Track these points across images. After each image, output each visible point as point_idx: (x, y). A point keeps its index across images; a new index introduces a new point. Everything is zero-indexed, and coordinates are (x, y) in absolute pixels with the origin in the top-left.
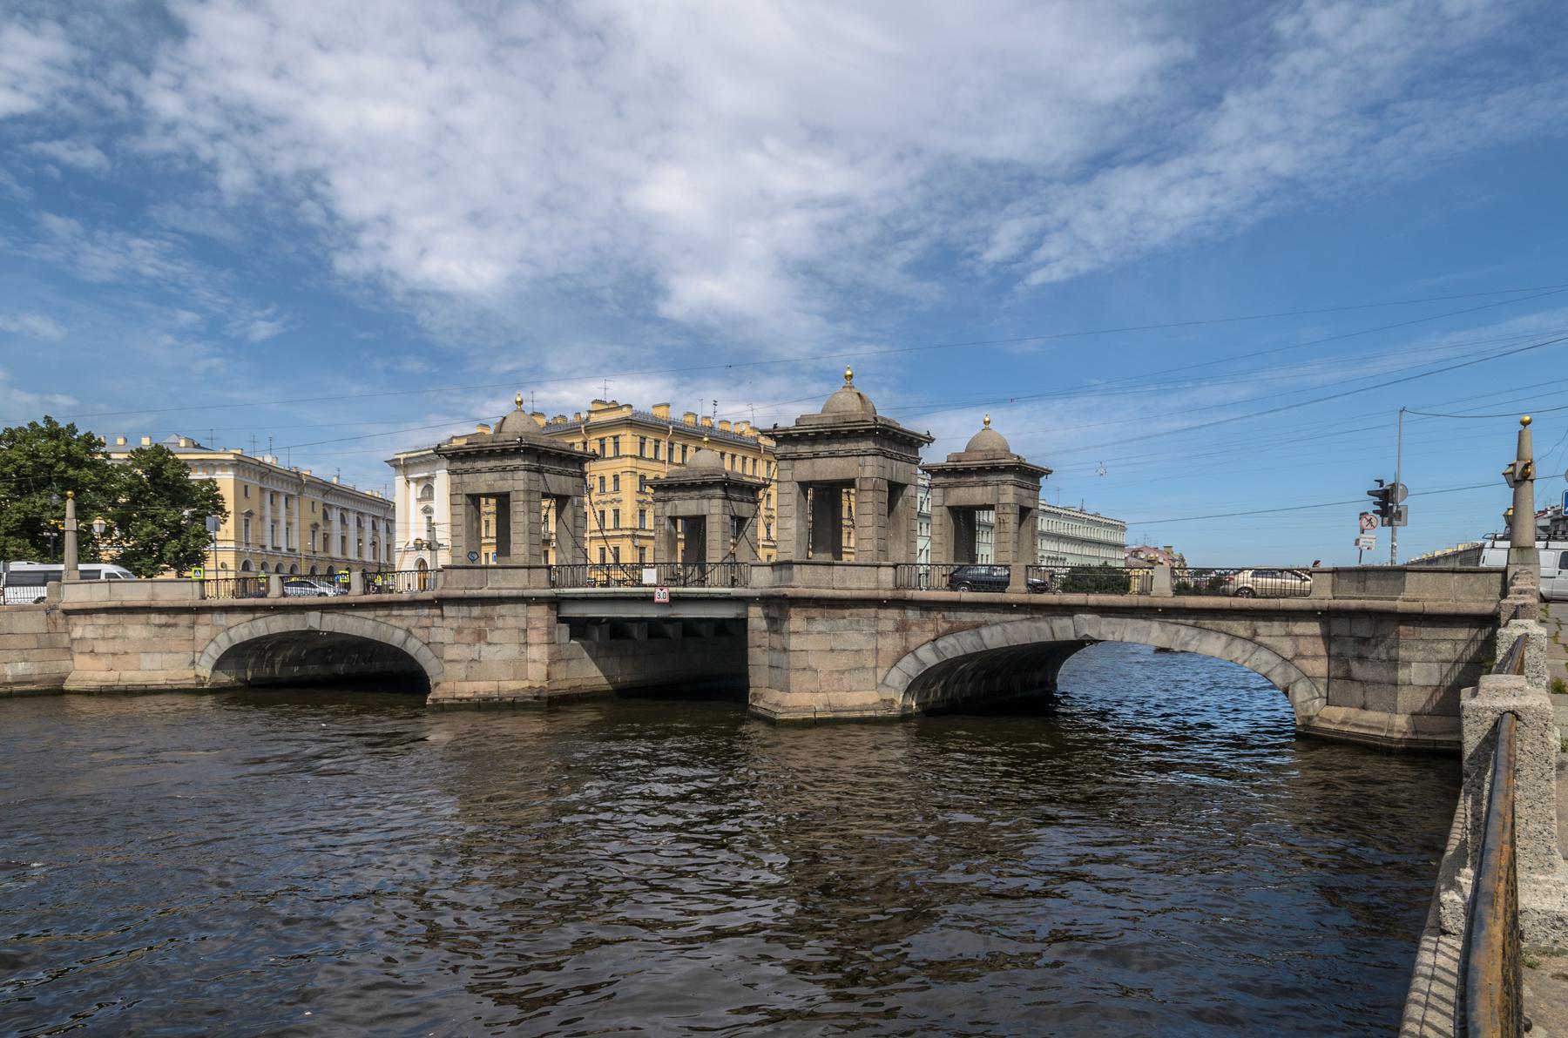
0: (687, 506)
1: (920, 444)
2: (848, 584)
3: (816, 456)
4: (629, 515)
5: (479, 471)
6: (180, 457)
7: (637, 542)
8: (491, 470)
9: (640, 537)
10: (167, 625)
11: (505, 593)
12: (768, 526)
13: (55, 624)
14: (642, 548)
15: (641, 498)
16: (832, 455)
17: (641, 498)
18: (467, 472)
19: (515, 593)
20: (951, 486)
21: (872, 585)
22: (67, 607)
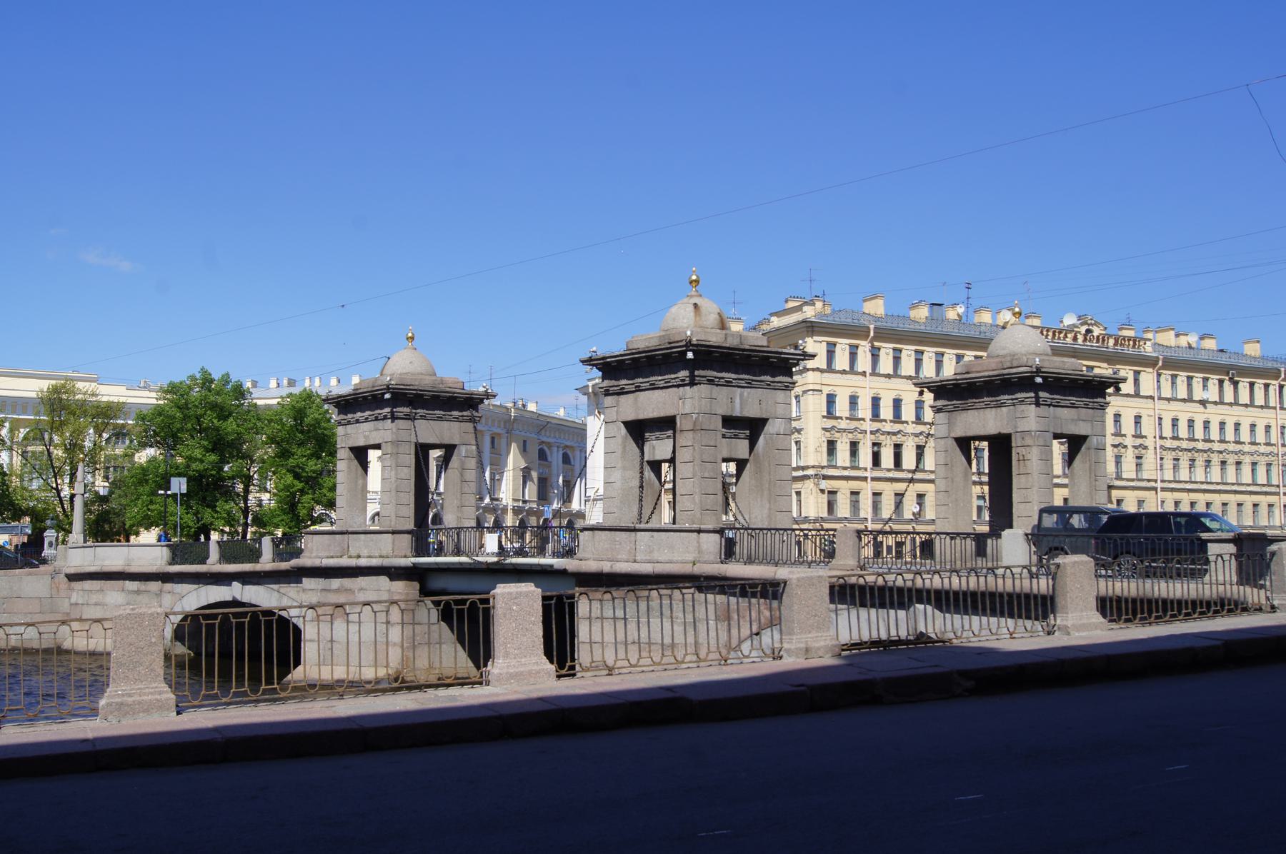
0: (985, 420)
1: (481, 401)
2: (656, 556)
3: (638, 389)
4: (811, 449)
5: (357, 422)
6: (260, 402)
7: (825, 484)
8: (367, 420)
9: (825, 477)
10: (138, 592)
11: (363, 562)
12: (1118, 460)
13: (1267, 598)
14: (832, 493)
15: (829, 424)
16: (653, 387)
17: (829, 424)
18: (349, 423)
19: (375, 562)
20: (956, 409)
21: (690, 557)
22: (72, 571)
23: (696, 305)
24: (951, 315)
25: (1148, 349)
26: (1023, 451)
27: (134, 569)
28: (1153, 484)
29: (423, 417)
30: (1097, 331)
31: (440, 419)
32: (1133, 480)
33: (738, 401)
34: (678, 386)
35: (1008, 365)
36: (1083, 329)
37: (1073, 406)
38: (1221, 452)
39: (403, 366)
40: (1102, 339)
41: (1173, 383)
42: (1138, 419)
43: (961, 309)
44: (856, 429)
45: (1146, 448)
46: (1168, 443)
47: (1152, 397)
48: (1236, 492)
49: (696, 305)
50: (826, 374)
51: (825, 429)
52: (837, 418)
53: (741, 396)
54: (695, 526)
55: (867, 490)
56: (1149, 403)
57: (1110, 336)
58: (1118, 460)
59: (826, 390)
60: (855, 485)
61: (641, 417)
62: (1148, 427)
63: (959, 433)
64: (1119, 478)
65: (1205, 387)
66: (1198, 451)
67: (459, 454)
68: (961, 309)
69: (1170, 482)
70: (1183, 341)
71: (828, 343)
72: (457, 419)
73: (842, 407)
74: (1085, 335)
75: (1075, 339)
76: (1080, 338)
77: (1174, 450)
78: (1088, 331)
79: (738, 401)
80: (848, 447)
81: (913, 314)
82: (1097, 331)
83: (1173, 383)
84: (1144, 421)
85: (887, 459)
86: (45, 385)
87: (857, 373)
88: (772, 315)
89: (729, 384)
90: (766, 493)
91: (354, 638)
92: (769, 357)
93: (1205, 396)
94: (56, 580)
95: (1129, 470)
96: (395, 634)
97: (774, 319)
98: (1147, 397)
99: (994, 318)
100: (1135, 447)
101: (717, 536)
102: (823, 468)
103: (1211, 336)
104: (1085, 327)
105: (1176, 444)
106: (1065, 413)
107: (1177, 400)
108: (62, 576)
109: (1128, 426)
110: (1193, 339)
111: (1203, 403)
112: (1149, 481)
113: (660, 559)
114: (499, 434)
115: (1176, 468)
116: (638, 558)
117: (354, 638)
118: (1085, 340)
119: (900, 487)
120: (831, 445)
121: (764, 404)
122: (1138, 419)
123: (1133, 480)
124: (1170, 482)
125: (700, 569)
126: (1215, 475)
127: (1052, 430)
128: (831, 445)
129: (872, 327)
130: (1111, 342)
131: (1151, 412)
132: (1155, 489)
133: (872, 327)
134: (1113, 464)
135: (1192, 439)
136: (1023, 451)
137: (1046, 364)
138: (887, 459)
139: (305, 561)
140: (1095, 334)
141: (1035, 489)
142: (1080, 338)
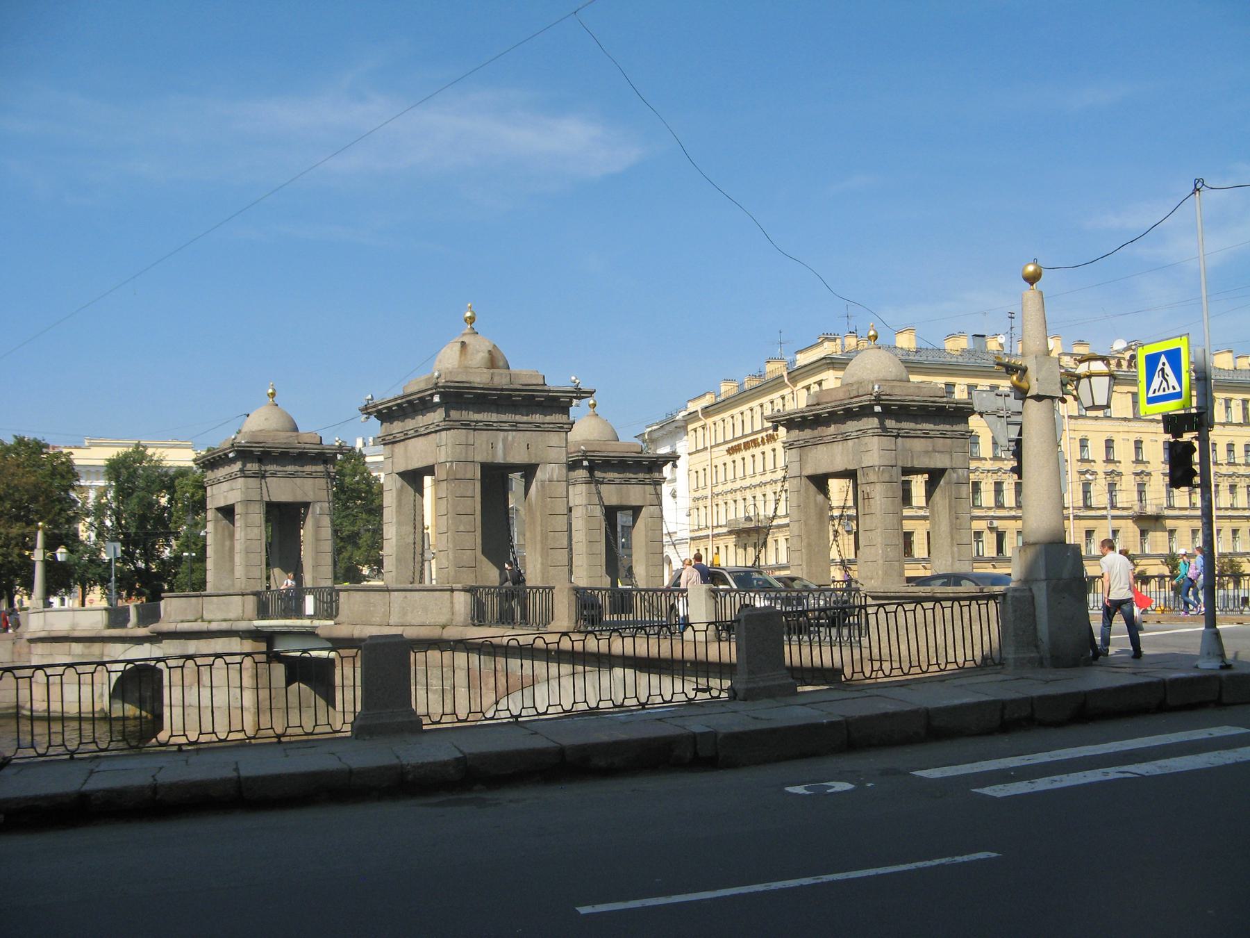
2: (410, 618)
11: (214, 626)
12: (1112, 488)
19: (225, 626)
21: (443, 619)
23: (463, 344)
26: (867, 489)
27: (77, 634)
29: (274, 475)
31: (293, 475)
32: (1186, 509)
33: (500, 445)
34: (436, 432)
35: (854, 393)
36: (1127, 355)
37: (926, 436)
39: (259, 423)
41: (1228, 407)
42: (1109, 444)
43: (1002, 339)
49: (463, 344)
53: (505, 440)
54: (447, 586)
56: (1124, 426)
58: (1112, 488)
61: (410, 468)
63: (810, 471)
64: (1170, 507)
67: (314, 513)
68: (1002, 339)
69: (1226, 509)
72: (310, 475)
74: (1130, 362)
75: (1119, 365)
76: (1124, 364)
77: (1230, 476)
79: (500, 445)
81: (949, 345)
83: (1228, 407)
86: (112, 453)
88: (797, 352)
89: (488, 427)
90: (539, 546)
91: (206, 702)
92: (559, 397)
94: (18, 645)
96: (249, 699)
97: (798, 356)
101: (468, 595)
104: (1131, 352)
105: (1232, 470)
106: (918, 445)
107: (1231, 424)
108: (24, 641)
109: (1096, 451)
112: (1124, 509)
113: (414, 622)
116: (391, 622)
117: (206, 702)
118: (1129, 366)
121: (532, 449)
122: (1109, 444)
123: (1186, 509)
124: (1226, 509)
125: (452, 633)
127: (900, 464)
136: (867, 489)
137: (897, 391)
139: (164, 626)
141: (879, 530)
142: (1124, 364)
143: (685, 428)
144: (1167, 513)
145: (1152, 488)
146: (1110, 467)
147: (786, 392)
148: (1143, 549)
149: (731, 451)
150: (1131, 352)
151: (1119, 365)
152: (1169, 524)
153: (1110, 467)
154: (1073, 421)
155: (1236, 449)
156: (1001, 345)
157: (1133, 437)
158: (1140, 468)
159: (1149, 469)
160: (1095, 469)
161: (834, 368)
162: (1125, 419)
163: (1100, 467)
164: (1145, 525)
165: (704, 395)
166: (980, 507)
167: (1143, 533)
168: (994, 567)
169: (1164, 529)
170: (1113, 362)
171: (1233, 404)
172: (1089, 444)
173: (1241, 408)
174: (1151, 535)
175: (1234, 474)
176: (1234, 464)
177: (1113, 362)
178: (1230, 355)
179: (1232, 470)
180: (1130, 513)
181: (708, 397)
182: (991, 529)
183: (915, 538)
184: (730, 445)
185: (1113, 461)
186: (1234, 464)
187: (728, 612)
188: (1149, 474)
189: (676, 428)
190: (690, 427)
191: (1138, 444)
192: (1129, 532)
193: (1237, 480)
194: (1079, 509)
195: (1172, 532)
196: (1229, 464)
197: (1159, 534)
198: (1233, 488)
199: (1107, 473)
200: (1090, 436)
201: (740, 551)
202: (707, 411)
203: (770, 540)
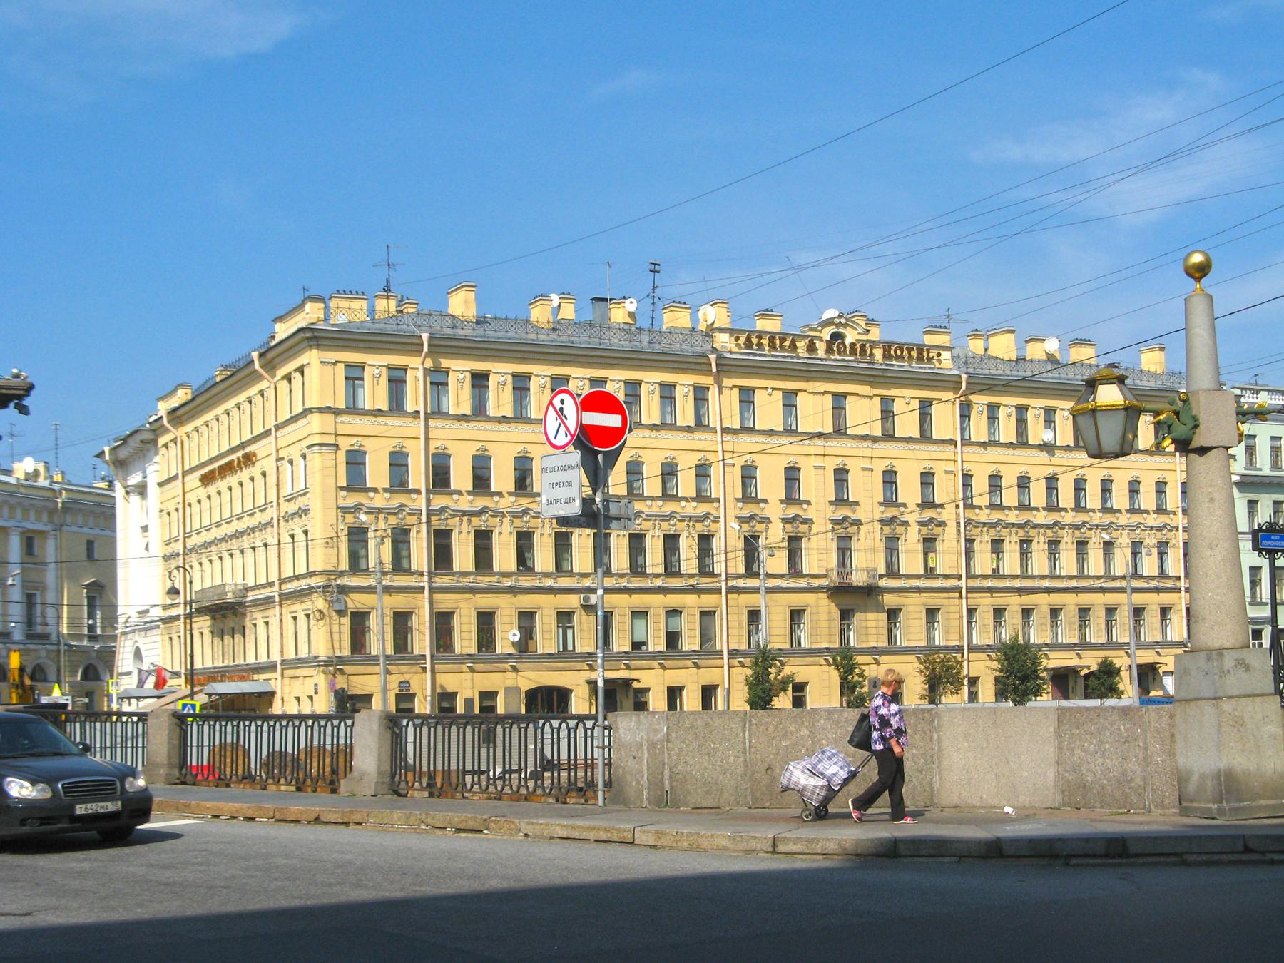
15: (351, 500)
24: (618, 315)
25: (946, 363)
28: (954, 582)
30: (851, 337)
38: (1077, 527)
40: (861, 349)
42: (927, 479)
43: (631, 305)
44: (401, 508)
45: (942, 524)
46: (983, 516)
47: (952, 442)
48: (1048, 591)
50: (513, 426)
51: (834, 522)
52: (368, 490)
55: (547, 608)
56: (866, 448)
57: (874, 344)
58: (929, 543)
59: (345, 444)
60: (400, 602)
62: (947, 489)
65: (1049, 422)
66: (1036, 526)
68: (631, 305)
70: (1035, 351)
71: (348, 365)
73: (377, 473)
75: (811, 348)
76: (821, 347)
78: (837, 337)
80: (513, 540)
82: (851, 337)
83: (993, 418)
84: (716, 472)
85: (463, 555)
87: (530, 421)
93: (1048, 436)
95: (910, 561)
97: (278, 327)
98: (943, 442)
99: (694, 317)
100: (742, 520)
102: (342, 574)
103: (1087, 342)
105: (996, 516)
107: (997, 444)
110: (1052, 345)
111: (1049, 448)
112: (946, 577)
114: (42, 533)
115: (1025, 555)
118: (829, 350)
119: (400, 602)
120: (358, 536)
123: (918, 577)
124: (985, 577)
126: (1067, 562)
128: (358, 536)
129: (425, 336)
130: (878, 353)
131: (950, 467)
132: (959, 590)
133: (425, 336)
134: (693, 553)
135: (1024, 507)
138: (463, 555)
140: (848, 341)
142: (821, 347)
143: (155, 442)
144: (882, 583)
145: (861, 544)
146: (792, 511)
147: (263, 385)
148: (1083, 636)
149: (207, 479)
150: (832, 329)
151: (811, 348)
152: (889, 600)
153: (792, 511)
154: (728, 437)
155: (974, 482)
156: (631, 314)
157: (831, 464)
158: (842, 512)
159: (860, 514)
160: (766, 514)
161: (318, 346)
162: (820, 435)
163: (775, 511)
164: (848, 602)
165: (176, 390)
166: (570, 573)
167: (845, 615)
168: (628, 667)
169: (879, 608)
170: (802, 345)
171: (1002, 413)
172: (936, 480)
173: (1013, 419)
174: (857, 618)
175: (999, 522)
176: (1000, 507)
177: (802, 345)
178: (1012, 336)
179: (996, 516)
180: (824, 582)
181: (181, 392)
182: (589, 609)
183: (457, 621)
184: (203, 471)
185: (799, 502)
186: (1000, 507)
187: (329, 741)
188: (858, 523)
189: (135, 448)
190: (161, 441)
191: (841, 476)
192: (822, 611)
193: (1004, 532)
194: (738, 577)
195: (893, 614)
196: (992, 506)
197: (871, 616)
198: (997, 544)
199: (785, 521)
200: (899, 466)
201: (217, 640)
202: (178, 416)
203: (248, 624)
